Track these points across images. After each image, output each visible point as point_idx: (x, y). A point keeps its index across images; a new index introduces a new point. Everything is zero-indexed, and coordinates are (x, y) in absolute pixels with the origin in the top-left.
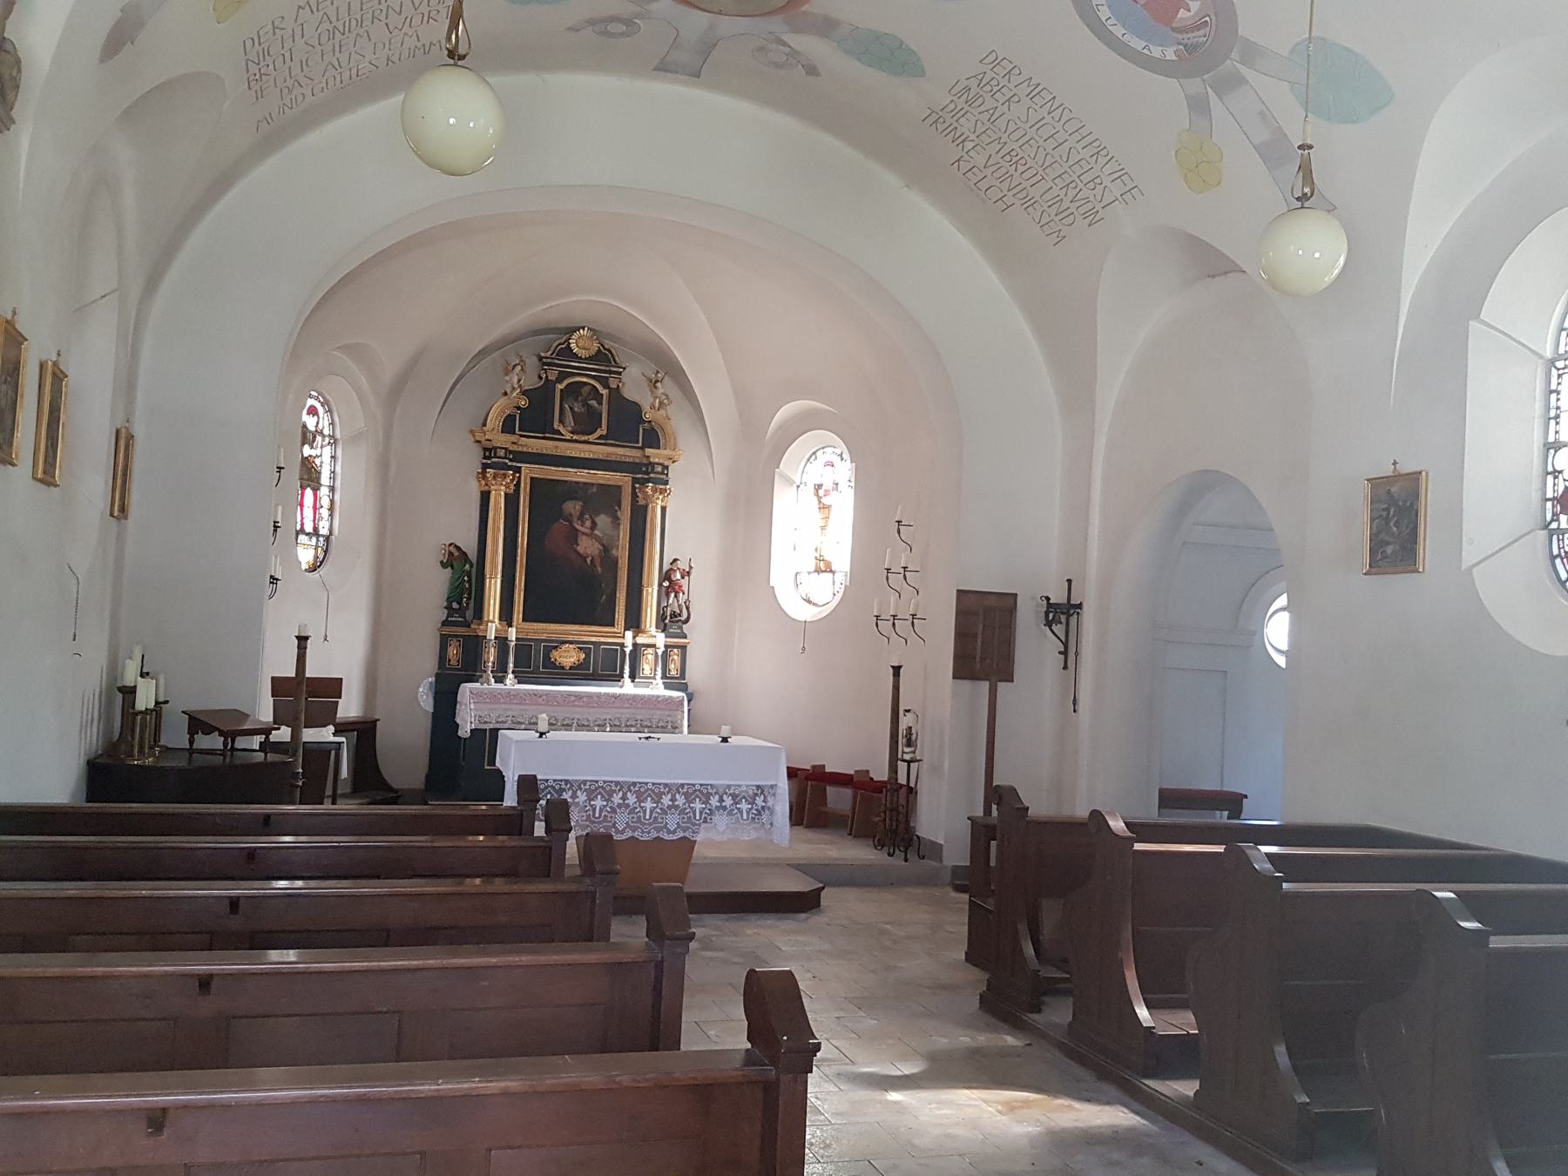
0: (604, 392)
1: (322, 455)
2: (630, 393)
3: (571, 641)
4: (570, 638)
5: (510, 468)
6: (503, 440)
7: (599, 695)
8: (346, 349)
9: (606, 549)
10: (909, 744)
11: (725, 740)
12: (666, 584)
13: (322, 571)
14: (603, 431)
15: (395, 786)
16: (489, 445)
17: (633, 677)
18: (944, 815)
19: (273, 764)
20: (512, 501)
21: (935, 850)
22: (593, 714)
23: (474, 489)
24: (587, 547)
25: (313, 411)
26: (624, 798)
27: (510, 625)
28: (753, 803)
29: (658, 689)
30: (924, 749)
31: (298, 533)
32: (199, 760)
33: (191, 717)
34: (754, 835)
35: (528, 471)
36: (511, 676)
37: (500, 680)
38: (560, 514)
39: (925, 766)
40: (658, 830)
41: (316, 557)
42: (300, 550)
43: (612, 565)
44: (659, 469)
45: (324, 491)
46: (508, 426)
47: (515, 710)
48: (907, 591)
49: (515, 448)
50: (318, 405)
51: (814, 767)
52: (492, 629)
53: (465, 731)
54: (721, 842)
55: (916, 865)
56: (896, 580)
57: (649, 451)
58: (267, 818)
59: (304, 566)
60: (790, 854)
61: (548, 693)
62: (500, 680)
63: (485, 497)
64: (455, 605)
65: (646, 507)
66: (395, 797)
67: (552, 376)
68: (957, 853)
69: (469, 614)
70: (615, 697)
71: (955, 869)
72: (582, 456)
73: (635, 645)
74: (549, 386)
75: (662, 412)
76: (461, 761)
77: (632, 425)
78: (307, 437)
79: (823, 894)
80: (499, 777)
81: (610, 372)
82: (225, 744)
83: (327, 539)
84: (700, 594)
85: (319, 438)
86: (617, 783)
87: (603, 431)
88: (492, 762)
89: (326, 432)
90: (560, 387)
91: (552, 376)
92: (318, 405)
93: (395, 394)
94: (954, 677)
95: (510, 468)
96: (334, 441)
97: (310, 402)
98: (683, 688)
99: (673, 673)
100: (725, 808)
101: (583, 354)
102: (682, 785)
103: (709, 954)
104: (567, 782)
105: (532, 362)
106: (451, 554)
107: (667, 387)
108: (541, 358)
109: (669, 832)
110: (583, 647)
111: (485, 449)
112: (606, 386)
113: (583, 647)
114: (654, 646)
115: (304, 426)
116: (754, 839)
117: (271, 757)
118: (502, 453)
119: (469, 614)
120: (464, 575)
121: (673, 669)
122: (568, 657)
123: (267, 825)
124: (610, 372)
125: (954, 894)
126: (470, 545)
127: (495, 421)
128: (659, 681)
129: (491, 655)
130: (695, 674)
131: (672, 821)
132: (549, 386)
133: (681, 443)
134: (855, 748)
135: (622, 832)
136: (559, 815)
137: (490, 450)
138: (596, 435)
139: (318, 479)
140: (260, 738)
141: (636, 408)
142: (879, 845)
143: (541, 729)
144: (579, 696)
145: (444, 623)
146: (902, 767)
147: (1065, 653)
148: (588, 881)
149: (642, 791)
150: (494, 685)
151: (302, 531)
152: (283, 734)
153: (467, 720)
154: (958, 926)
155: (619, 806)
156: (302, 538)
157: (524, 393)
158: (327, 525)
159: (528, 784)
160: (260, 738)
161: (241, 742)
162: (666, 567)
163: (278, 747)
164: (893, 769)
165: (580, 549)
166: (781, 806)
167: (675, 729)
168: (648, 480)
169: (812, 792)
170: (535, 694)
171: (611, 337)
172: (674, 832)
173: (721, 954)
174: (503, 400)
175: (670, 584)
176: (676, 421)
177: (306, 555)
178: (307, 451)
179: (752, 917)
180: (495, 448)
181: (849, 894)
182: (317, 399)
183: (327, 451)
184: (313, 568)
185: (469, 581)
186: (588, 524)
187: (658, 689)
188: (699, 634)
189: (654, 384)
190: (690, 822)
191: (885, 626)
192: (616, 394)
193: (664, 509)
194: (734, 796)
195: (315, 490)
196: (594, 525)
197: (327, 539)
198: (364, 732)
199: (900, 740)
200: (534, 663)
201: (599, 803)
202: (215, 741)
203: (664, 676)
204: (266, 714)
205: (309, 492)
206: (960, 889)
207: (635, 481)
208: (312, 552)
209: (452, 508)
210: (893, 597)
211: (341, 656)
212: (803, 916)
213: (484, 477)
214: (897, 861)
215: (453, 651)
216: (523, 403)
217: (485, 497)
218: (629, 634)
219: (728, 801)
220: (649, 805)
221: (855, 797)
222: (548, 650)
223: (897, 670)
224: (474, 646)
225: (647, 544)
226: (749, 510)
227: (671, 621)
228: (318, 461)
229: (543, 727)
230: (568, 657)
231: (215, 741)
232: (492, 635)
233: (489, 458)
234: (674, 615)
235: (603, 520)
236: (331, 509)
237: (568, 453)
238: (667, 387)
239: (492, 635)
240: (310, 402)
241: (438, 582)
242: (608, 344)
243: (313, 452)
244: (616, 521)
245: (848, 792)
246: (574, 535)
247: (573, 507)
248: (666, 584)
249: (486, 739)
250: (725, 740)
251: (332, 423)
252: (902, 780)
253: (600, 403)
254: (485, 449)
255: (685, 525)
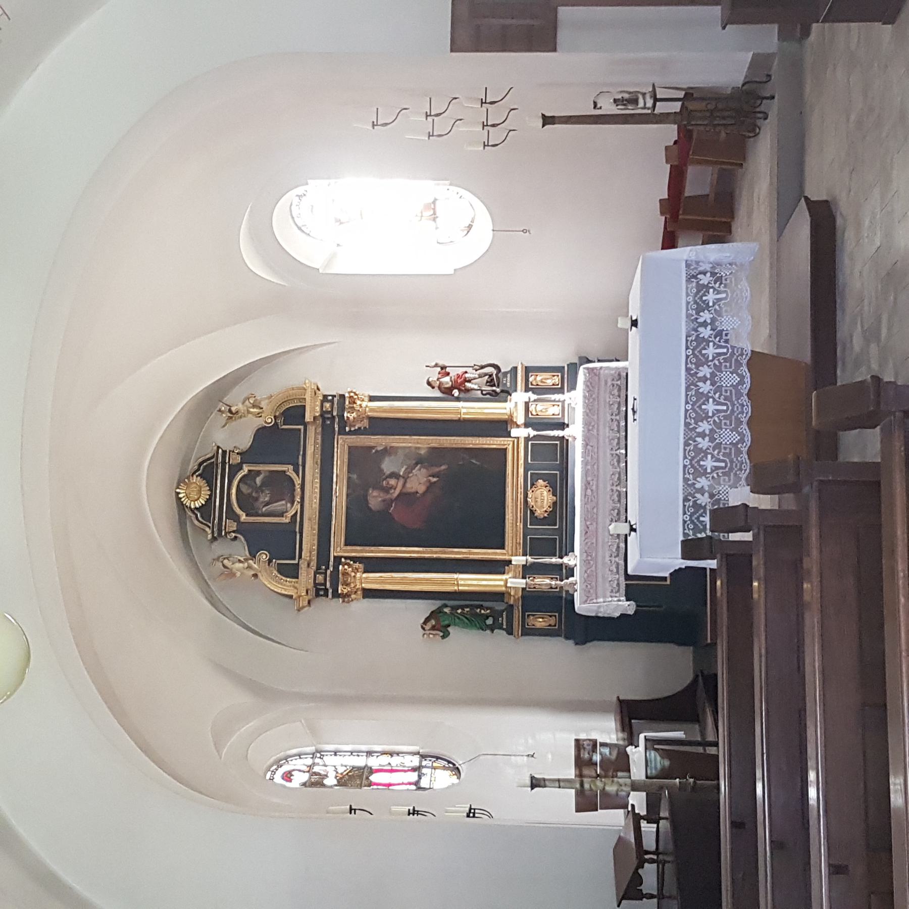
0: (246, 469)
1: (333, 767)
2: (245, 441)
3: (525, 496)
4: (521, 496)
5: (336, 568)
6: (306, 577)
7: (585, 463)
8: (218, 746)
9: (420, 461)
10: (635, 101)
11: (634, 323)
12: (456, 393)
13: (459, 762)
14: (289, 469)
15: (688, 680)
16: (312, 592)
17: (562, 426)
18: (717, 56)
19: (672, 812)
20: (372, 565)
21: (760, 63)
22: (607, 470)
23: (361, 606)
24: (418, 482)
25: (288, 777)
26: (703, 435)
27: (510, 561)
28: (707, 287)
29: (576, 398)
30: (639, 82)
31: (419, 788)
32: (671, 886)
33: (623, 898)
34: (744, 284)
35: (338, 548)
36: (565, 560)
37: (570, 572)
38: (384, 514)
39: (658, 81)
40: (739, 395)
41: (444, 768)
42: (437, 786)
43: (437, 453)
44: (327, 405)
45: (374, 762)
46: (291, 572)
47: (605, 555)
48: (454, 111)
49: (314, 564)
50: (281, 771)
51: (662, 213)
52: (512, 582)
53: (629, 607)
54: (750, 323)
55: (776, 87)
56: (441, 125)
57: (308, 418)
58: (736, 825)
59: (454, 779)
60: (766, 238)
61: (585, 519)
62: (570, 572)
63: (369, 594)
64: (490, 621)
65: (370, 419)
66: (705, 682)
67: (232, 526)
68: (766, 38)
69: (499, 606)
70: (586, 445)
71: (782, 36)
72: (316, 492)
73: (526, 425)
74: (243, 529)
75: (263, 404)
76: (662, 611)
77: (281, 435)
78: (316, 782)
79: (814, 198)
80: (677, 574)
81: (224, 463)
82: (652, 861)
83: (423, 757)
84: (466, 354)
85: (316, 769)
86: (686, 444)
87: (289, 469)
88: (665, 579)
89: (309, 761)
90: (243, 517)
91: (232, 526)
92: (281, 771)
93: (263, 692)
94: (554, 50)
95: (336, 568)
96: (319, 753)
97: (278, 779)
98: (573, 368)
99: (557, 380)
100: (713, 320)
101: (206, 493)
102: (688, 370)
103: (884, 332)
104: (686, 500)
105: (219, 548)
106: (433, 628)
107: (235, 399)
108: (214, 539)
109: (741, 382)
110: (531, 481)
111: (317, 595)
112: (239, 467)
113: (531, 481)
114: (527, 404)
115: (304, 784)
116: (748, 278)
117: (664, 813)
118: (320, 578)
119: (499, 606)
120: (455, 613)
121: (551, 380)
122: (542, 498)
123: (744, 824)
124: (224, 463)
125: (813, 37)
126: (424, 608)
127: (285, 586)
128: (566, 396)
129: (543, 582)
130: (554, 352)
131: (728, 379)
132: (243, 529)
133: (296, 383)
134: (640, 163)
135: (742, 435)
136: (728, 517)
137: (318, 590)
138: (293, 475)
139: (359, 768)
140: (643, 824)
141: (261, 433)
142: (754, 131)
143: (627, 531)
144: (586, 485)
145: (510, 632)
146: (661, 108)
147: (398, 754)
148: (806, 489)
149: (696, 415)
150: (577, 577)
151: (416, 783)
152: (638, 800)
153: (617, 605)
154: (851, 34)
155: (712, 440)
156: (424, 783)
157: (253, 556)
158: (408, 758)
159: (690, 548)
160: (643, 824)
161: (649, 843)
162: (438, 394)
163: (653, 804)
164: (663, 118)
165: (421, 489)
166: (712, 253)
167: (623, 378)
168: (341, 417)
169: (693, 215)
170: (585, 532)
171: (186, 461)
172: (742, 377)
173: (885, 318)
174: (264, 579)
175: (456, 389)
176: (271, 389)
177: (442, 779)
178: (331, 781)
179: (840, 279)
180: (315, 584)
181: (812, 163)
182: (274, 772)
183: (329, 760)
184: (457, 771)
185: (462, 607)
186: (392, 482)
187: (576, 398)
188: (510, 354)
189: (233, 415)
190: (731, 359)
191: (496, 135)
192: (247, 456)
193: (372, 399)
194: (699, 310)
195: (372, 771)
196: (394, 475)
197: (423, 757)
198: (631, 714)
199: (629, 112)
200: (551, 536)
201: (709, 463)
202: (649, 872)
203: (561, 391)
204: (615, 818)
205: (374, 778)
206: (806, 32)
207: (342, 432)
208: (439, 772)
209: (383, 628)
210: (461, 128)
211: (551, 740)
212: (839, 221)
213: (348, 595)
214: (774, 108)
215: (540, 622)
216: (264, 556)
217: (369, 594)
218: (515, 432)
219: (706, 316)
220: (710, 407)
221: (699, 162)
222: (535, 520)
223: (547, 120)
224: (533, 601)
225: (410, 415)
226: (363, 305)
227: (498, 385)
228: (341, 770)
229: (623, 528)
230: (542, 498)
231: (649, 872)
232: (521, 583)
233: (326, 590)
234: (491, 383)
235: (388, 466)
236: (391, 754)
237: (316, 506)
238: (235, 399)
239: (521, 583)
240: (278, 779)
241: (463, 639)
242: (192, 466)
243: (332, 774)
244: (387, 451)
245: (692, 171)
246: (406, 497)
247: (375, 499)
248: (456, 393)
249: (636, 587)
250: (634, 323)
251: (299, 755)
252: (676, 107)
253: (258, 473)
254: (317, 595)
255: (389, 373)
